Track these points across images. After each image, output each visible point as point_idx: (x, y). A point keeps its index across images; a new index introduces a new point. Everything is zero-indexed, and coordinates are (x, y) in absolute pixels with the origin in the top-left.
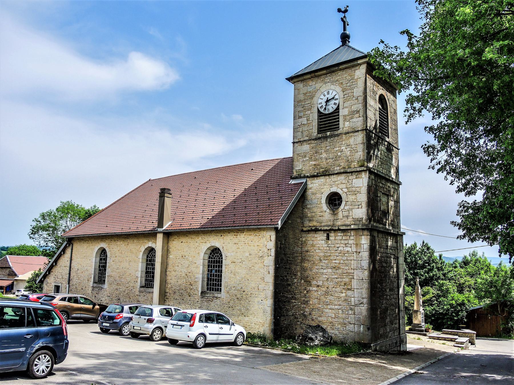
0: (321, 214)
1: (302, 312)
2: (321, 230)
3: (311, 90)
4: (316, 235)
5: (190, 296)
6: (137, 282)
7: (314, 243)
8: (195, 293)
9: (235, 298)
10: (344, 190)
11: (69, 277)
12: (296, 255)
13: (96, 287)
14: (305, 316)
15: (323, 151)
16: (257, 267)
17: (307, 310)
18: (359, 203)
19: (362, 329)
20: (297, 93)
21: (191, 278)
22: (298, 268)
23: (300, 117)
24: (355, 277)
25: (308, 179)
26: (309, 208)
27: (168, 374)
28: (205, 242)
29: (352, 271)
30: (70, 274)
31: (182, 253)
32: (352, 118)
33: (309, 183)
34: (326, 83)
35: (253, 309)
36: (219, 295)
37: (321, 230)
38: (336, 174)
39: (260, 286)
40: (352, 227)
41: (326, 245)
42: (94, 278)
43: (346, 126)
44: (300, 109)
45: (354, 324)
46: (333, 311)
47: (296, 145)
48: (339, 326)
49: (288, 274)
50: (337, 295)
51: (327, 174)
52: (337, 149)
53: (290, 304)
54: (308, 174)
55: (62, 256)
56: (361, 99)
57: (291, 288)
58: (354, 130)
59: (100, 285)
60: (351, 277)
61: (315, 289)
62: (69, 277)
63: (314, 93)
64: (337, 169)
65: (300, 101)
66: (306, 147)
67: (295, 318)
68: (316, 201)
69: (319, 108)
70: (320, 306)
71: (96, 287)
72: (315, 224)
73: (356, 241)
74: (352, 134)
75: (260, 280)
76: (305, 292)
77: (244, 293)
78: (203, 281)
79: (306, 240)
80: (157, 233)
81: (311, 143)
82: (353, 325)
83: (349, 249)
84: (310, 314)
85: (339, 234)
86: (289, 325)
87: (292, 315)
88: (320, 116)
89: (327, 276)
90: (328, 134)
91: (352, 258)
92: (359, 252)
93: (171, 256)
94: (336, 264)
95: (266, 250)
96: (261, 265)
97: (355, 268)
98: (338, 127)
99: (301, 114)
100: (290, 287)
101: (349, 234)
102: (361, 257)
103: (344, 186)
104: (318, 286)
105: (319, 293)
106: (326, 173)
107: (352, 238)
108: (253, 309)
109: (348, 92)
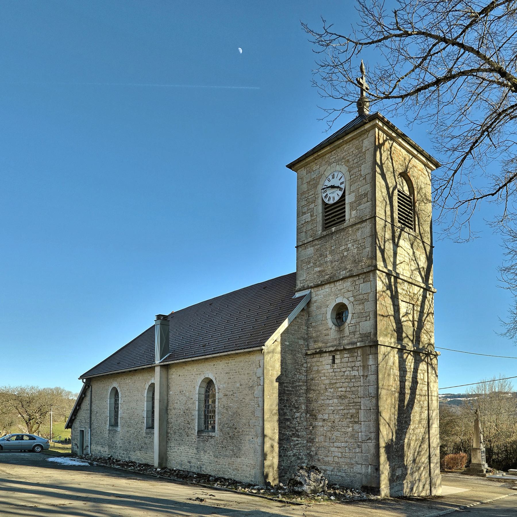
0: (327, 332)
1: (308, 452)
2: (326, 352)
3: (315, 176)
4: (321, 359)
5: (188, 436)
6: (143, 423)
7: (320, 369)
8: (192, 432)
9: (227, 436)
10: (350, 299)
11: (91, 421)
12: (297, 384)
13: (112, 430)
14: (311, 456)
15: (328, 252)
16: (247, 399)
17: (313, 449)
18: (367, 314)
19: (369, 470)
20: (300, 184)
21: (188, 415)
22: (302, 400)
23: (304, 213)
24: (362, 408)
25: (312, 290)
26: (314, 327)
27: (290, 513)
28: (200, 374)
29: (358, 400)
30: (91, 417)
31: (180, 388)
32: (360, 204)
33: (313, 295)
34: (330, 164)
35: (244, 448)
36: (213, 434)
37: (326, 352)
38: (342, 279)
39: (250, 421)
40: (359, 344)
41: (332, 370)
42: (110, 420)
43: (353, 216)
44: (304, 203)
45: (362, 464)
46: (340, 450)
47: (300, 249)
48: (347, 467)
49: (285, 406)
50: (343, 430)
51: (332, 280)
52: (343, 247)
53: (290, 442)
54: (312, 284)
55: (85, 399)
56: (369, 177)
57: (291, 423)
58: (361, 220)
59: (115, 428)
60: (358, 407)
61: (320, 424)
62: (91, 421)
63: (318, 180)
64: (343, 273)
65: (304, 193)
66: (310, 251)
67: (299, 458)
68: (321, 316)
69: (324, 198)
70: (326, 444)
71: (112, 430)
72: (320, 345)
73: (363, 362)
74: (359, 226)
75: (250, 414)
76: (311, 428)
77: (236, 431)
78: (199, 418)
79: (311, 365)
80: (155, 367)
81: (316, 245)
82: (360, 466)
83: (355, 373)
84: (316, 454)
85: (346, 355)
86: (289, 467)
87: (294, 455)
88: (326, 209)
89: (333, 408)
90: (333, 231)
91: (358, 384)
92: (367, 376)
93: (171, 393)
94: (342, 393)
95: (256, 379)
96: (251, 397)
97: (362, 395)
98: (345, 220)
99: (305, 209)
100: (289, 423)
101: (356, 354)
102: (369, 382)
103: (350, 294)
104: (324, 420)
105: (325, 428)
106: (332, 281)
107: (359, 358)
108: (244, 448)
109: (355, 171)
